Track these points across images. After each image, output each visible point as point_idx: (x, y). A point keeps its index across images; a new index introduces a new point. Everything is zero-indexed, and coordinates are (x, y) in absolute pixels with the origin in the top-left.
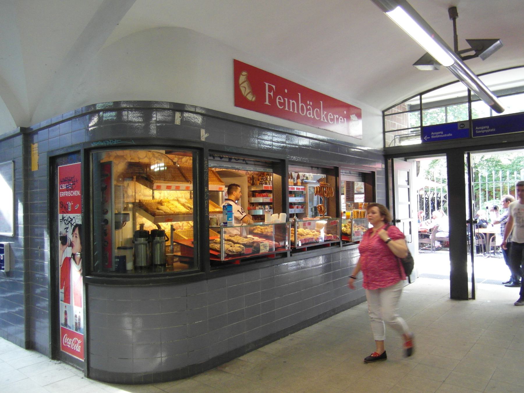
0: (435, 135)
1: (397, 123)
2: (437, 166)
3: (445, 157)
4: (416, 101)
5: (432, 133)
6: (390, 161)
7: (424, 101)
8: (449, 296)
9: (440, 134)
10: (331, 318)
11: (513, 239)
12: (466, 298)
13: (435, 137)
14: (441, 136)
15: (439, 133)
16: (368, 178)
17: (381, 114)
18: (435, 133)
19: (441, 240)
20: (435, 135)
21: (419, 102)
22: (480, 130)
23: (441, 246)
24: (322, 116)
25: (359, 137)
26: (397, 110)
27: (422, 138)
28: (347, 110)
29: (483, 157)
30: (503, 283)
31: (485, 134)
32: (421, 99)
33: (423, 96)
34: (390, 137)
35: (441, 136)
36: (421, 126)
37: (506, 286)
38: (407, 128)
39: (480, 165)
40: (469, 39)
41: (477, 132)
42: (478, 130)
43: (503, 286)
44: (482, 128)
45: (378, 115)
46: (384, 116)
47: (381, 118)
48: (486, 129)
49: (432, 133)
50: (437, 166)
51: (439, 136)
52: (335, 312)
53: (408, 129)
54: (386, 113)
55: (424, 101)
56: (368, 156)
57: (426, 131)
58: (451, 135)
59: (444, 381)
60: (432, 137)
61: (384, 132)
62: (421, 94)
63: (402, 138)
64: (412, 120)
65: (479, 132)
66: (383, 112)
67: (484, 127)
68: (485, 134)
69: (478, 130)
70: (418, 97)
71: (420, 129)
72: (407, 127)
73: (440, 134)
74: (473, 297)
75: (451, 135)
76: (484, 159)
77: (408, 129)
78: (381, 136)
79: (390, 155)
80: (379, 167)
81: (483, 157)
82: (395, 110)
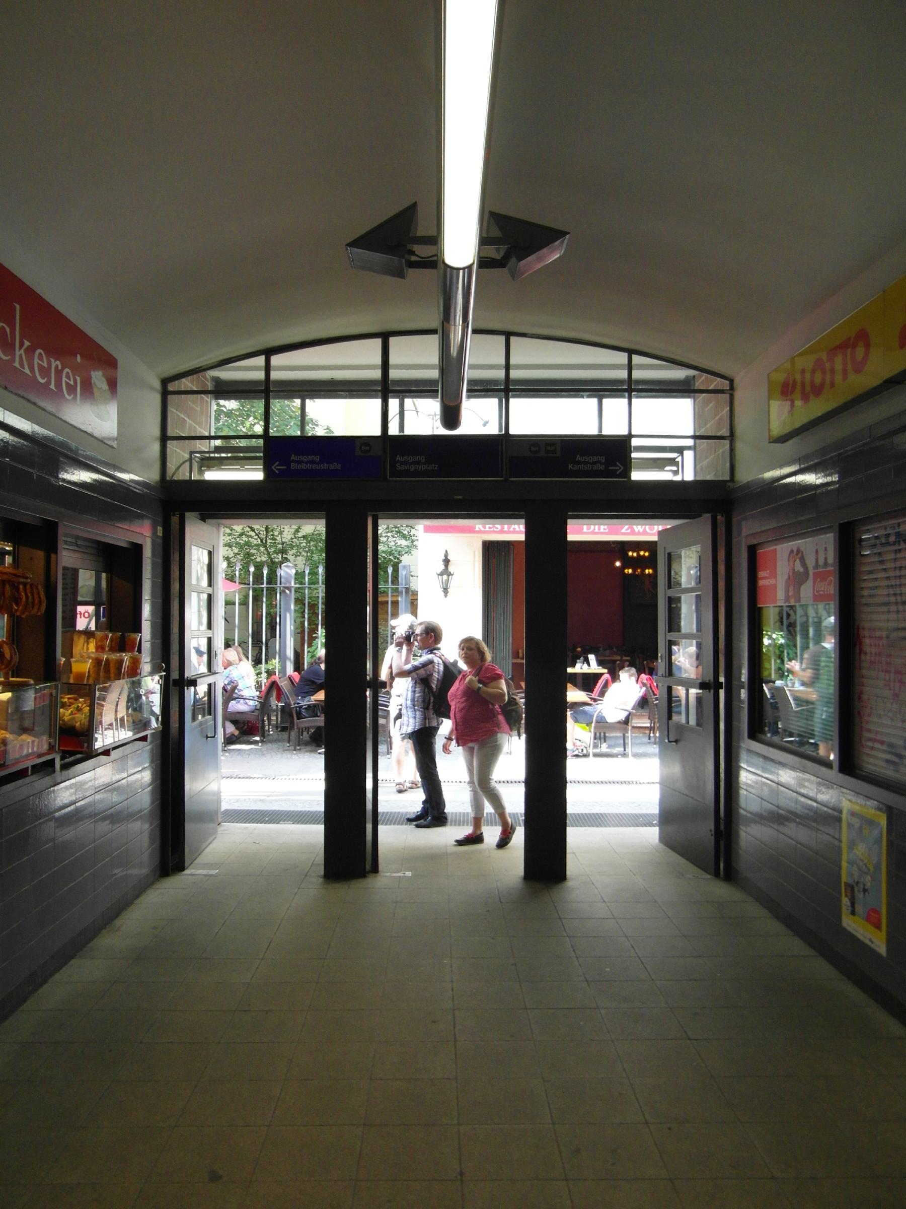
0: (299, 462)
1: (188, 420)
2: (299, 542)
3: (324, 521)
4: (250, 370)
5: (293, 457)
6: (175, 520)
7: (275, 375)
8: (321, 871)
9: (313, 462)
10: (25, 1007)
11: (192, 689)
12: (362, 874)
13: (300, 467)
14: (314, 466)
15: (310, 458)
16: (120, 563)
17: (157, 385)
18: (302, 458)
19: (238, 717)
20: (299, 462)
21: (260, 375)
22: (406, 463)
23: (237, 733)
24: (18, 353)
25: (110, 443)
26: (190, 385)
27: (267, 470)
28: (84, 357)
29: (297, 531)
30: (410, 820)
31: (416, 474)
32: (268, 368)
33: (276, 360)
34: (178, 452)
35: (314, 466)
36: (266, 435)
37: (418, 826)
38: (223, 435)
39: (292, 547)
40: (503, 212)
41: (399, 467)
42: (402, 463)
43: (411, 828)
44: (411, 459)
45: (152, 388)
46: (165, 394)
47: (157, 398)
48: (418, 463)
49: (293, 457)
50: (299, 542)
51: (309, 466)
52: (37, 980)
53: (210, 438)
54: (171, 387)
55: (275, 375)
56: (112, 500)
57: (278, 451)
58: (339, 467)
59: (461, 1174)
60: (293, 466)
61: (164, 438)
62: (269, 352)
63: (208, 462)
64: (242, 418)
65: (404, 467)
66: (165, 382)
67: (416, 458)
68: (416, 474)
69: (402, 463)
70: (260, 360)
71: (261, 442)
72: (207, 434)
73: (313, 462)
74: (375, 869)
75: (339, 467)
76: (300, 535)
77: (210, 438)
78: (156, 447)
79: (182, 503)
80: (143, 533)
81: (297, 531)
82: (186, 384)
